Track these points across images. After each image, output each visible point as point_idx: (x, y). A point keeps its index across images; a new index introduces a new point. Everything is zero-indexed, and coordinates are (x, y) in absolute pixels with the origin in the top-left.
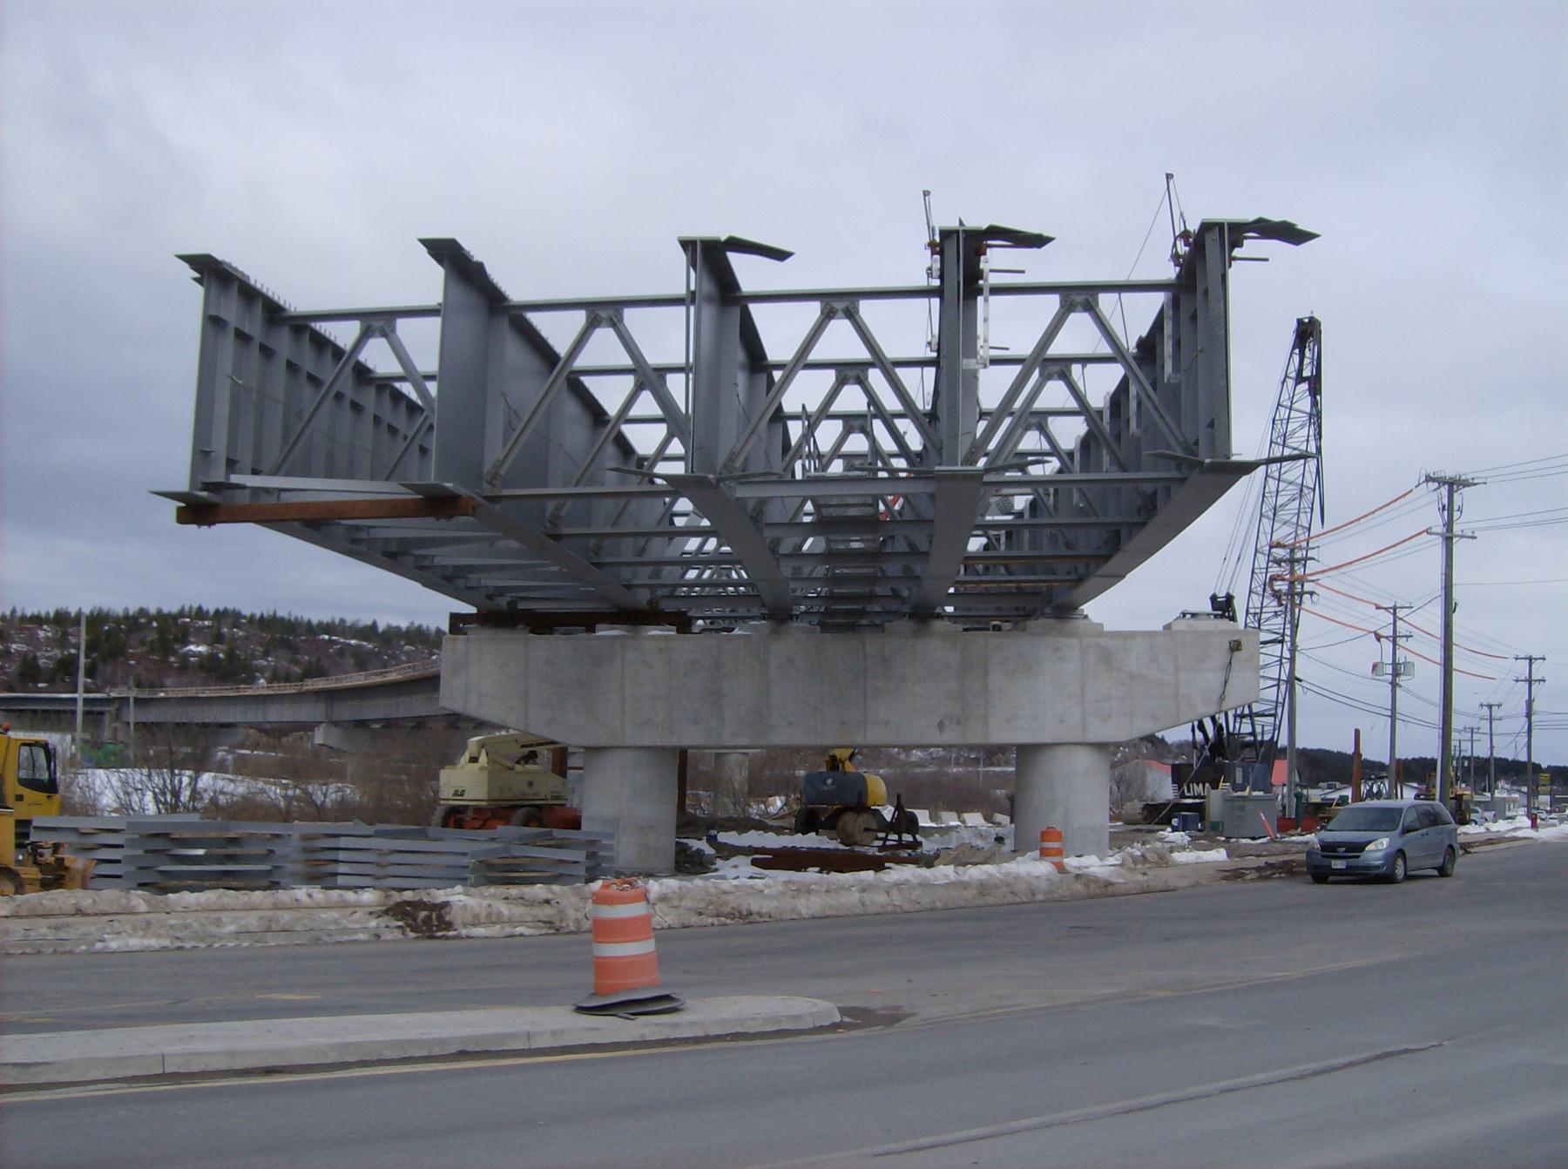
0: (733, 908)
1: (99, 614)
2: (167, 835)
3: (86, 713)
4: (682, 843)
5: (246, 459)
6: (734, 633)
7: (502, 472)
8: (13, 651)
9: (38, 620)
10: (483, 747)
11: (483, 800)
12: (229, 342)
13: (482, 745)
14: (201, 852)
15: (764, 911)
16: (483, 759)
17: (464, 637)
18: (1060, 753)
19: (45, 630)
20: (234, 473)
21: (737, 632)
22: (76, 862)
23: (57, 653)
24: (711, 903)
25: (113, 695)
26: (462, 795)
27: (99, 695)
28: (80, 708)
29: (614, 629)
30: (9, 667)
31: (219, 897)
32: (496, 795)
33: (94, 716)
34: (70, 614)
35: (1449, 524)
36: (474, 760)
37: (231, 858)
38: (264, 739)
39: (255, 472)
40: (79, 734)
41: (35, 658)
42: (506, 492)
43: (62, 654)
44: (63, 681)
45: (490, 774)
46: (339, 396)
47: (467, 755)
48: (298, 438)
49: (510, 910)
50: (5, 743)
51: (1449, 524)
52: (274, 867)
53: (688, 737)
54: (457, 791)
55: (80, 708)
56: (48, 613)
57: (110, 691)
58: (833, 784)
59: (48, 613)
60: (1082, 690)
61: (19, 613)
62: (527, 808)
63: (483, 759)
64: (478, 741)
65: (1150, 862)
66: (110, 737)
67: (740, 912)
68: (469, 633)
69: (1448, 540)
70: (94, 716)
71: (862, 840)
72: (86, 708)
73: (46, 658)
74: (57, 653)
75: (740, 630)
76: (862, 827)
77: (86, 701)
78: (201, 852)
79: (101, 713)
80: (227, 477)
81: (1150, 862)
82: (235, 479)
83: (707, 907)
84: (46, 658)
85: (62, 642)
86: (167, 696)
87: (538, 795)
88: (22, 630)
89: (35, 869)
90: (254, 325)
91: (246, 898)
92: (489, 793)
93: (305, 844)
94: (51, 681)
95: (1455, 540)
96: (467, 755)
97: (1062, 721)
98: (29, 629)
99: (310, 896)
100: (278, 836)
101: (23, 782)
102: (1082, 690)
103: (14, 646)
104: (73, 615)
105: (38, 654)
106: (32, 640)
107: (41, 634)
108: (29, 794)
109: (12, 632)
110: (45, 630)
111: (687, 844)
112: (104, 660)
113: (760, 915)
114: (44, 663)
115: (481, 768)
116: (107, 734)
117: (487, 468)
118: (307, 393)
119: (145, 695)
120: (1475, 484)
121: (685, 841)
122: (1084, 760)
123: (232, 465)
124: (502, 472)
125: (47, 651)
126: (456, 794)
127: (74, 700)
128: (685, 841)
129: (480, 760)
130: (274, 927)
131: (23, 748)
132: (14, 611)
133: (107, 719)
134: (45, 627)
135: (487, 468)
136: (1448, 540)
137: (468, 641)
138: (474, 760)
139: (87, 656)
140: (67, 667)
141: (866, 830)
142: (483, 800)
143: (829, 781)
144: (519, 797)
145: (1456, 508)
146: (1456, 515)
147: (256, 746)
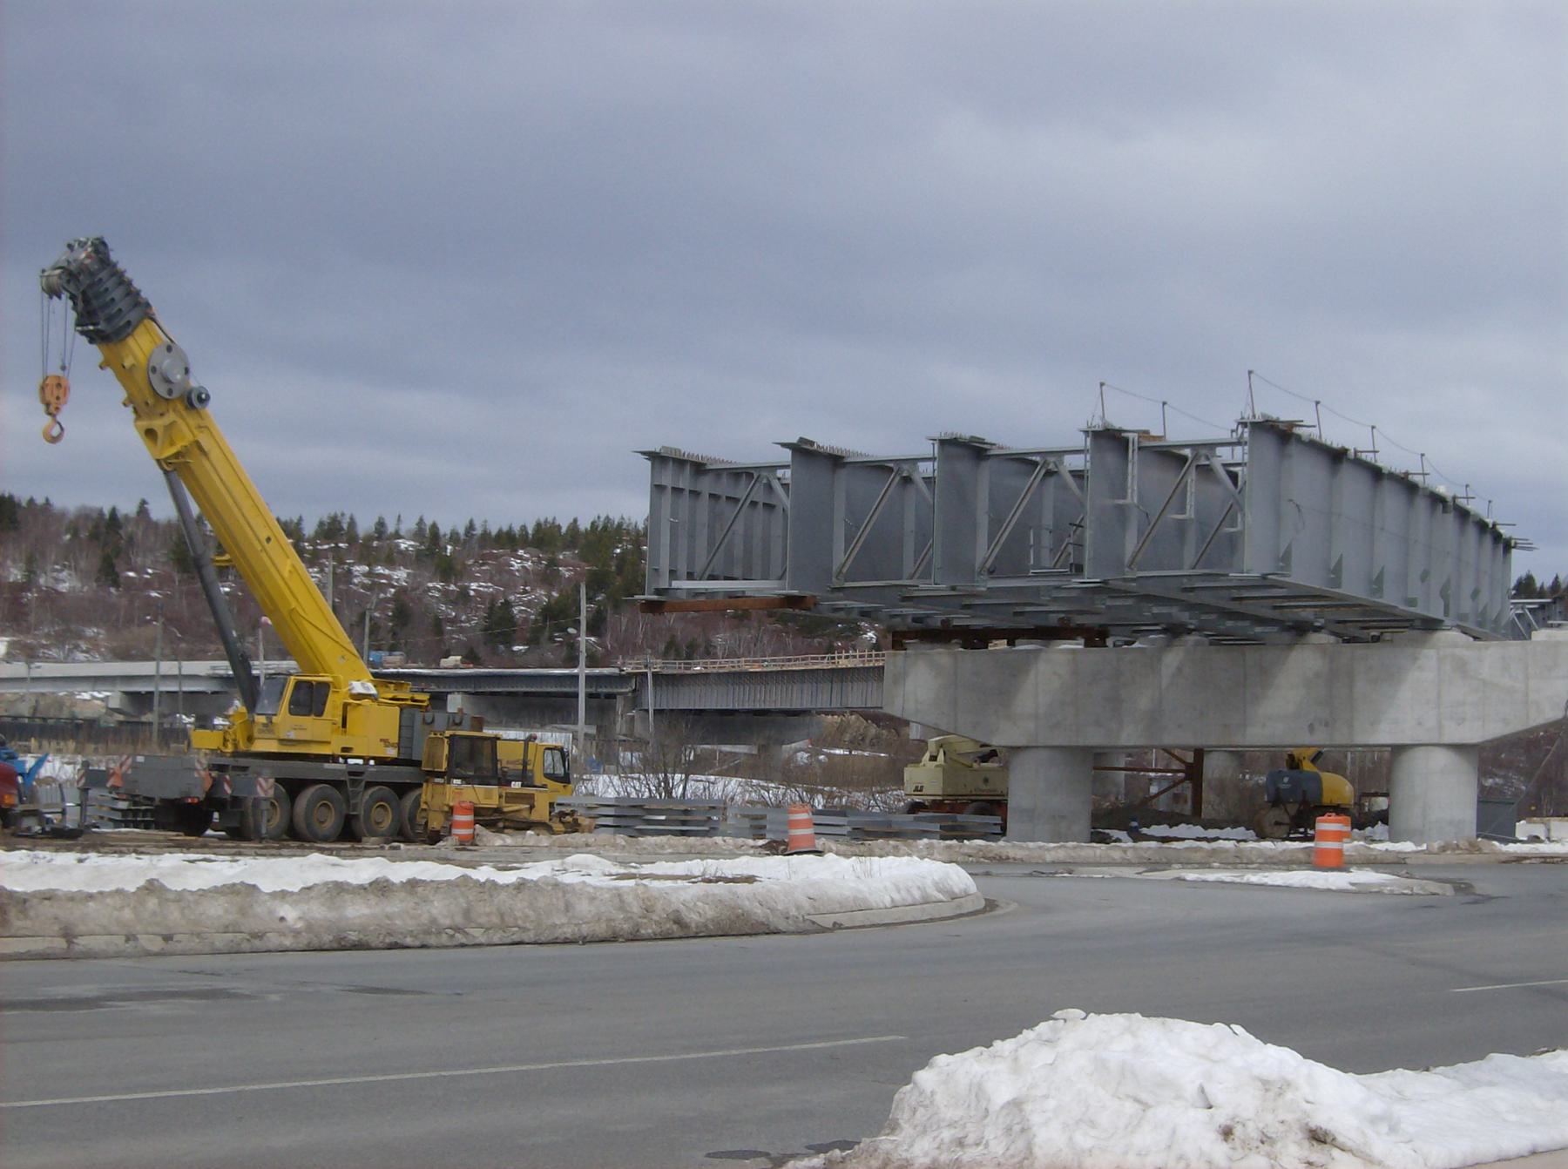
0: (996, 855)
1: (605, 528)
2: (641, 806)
3: (589, 696)
4: (1104, 833)
5: (683, 569)
6: (1134, 646)
7: (844, 570)
8: (472, 593)
9: (509, 540)
10: (941, 746)
11: (939, 795)
12: (668, 497)
13: (940, 745)
14: (663, 818)
15: (1018, 857)
16: (941, 757)
17: (904, 652)
18: (1419, 753)
19: (520, 558)
20: (675, 580)
21: (1136, 645)
22: (585, 821)
23: (541, 595)
24: (981, 851)
25: (628, 669)
26: (921, 791)
27: (606, 671)
28: (582, 691)
29: (1032, 644)
30: (468, 620)
31: (668, 840)
32: (950, 791)
33: (601, 705)
34: (559, 527)
36: (933, 758)
37: (684, 823)
38: (873, 730)
39: (690, 576)
40: (582, 727)
41: (508, 605)
42: (847, 585)
43: (549, 596)
44: (551, 639)
45: (945, 771)
46: (754, 504)
47: (927, 756)
48: (721, 543)
49: (837, 847)
50: (535, 747)
52: (711, 828)
53: (1094, 738)
54: (917, 787)
55: (582, 691)
56: (524, 528)
57: (624, 664)
58: (1288, 783)
59: (524, 528)
60: (1439, 696)
61: (478, 531)
62: (980, 803)
63: (941, 757)
64: (936, 741)
65: (1461, 849)
66: (624, 731)
67: (1000, 857)
68: (908, 647)
70: (601, 705)
71: (1272, 833)
72: (590, 690)
73: (526, 603)
74: (541, 593)
75: (1140, 643)
76: (1274, 821)
77: (588, 677)
78: (663, 818)
79: (611, 696)
80: (670, 585)
81: (1461, 849)
82: (675, 584)
83: (978, 853)
84: (526, 603)
85: (547, 577)
86: (704, 671)
87: (995, 791)
88: (485, 558)
89: (561, 825)
90: (685, 482)
91: (685, 841)
92: (944, 789)
93: (762, 822)
94: (533, 641)
96: (927, 756)
97: (1420, 724)
98: (496, 557)
99: (725, 841)
100: (714, 808)
101: (548, 776)
102: (1439, 696)
103: (474, 586)
104: (564, 530)
105: (512, 598)
106: (501, 574)
107: (516, 564)
108: (551, 783)
109: (470, 562)
110: (520, 558)
111: (1108, 834)
112: (617, 607)
113: (1015, 859)
114: (521, 611)
115: (937, 766)
116: (620, 726)
117: (835, 568)
118: (729, 511)
119: (675, 667)
121: (1107, 831)
122: (1441, 759)
123: (673, 574)
124: (844, 570)
125: (525, 592)
126: (916, 790)
127: (576, 677)
128: (1107, 831)
129: (938, 759)
130: (693, 851)
131: (547, 751)
132: (471, 527)
133: (620, 705)
134: (521, 552)
135: (835, 568)
137: (906, 656)
138: (933, 758)
139: (590, 600)
140: (557, 616)
141: (1277, 823)
142: (939, 795)
143: (1286, 780)
144: (974, 793)
147: (854, 744)
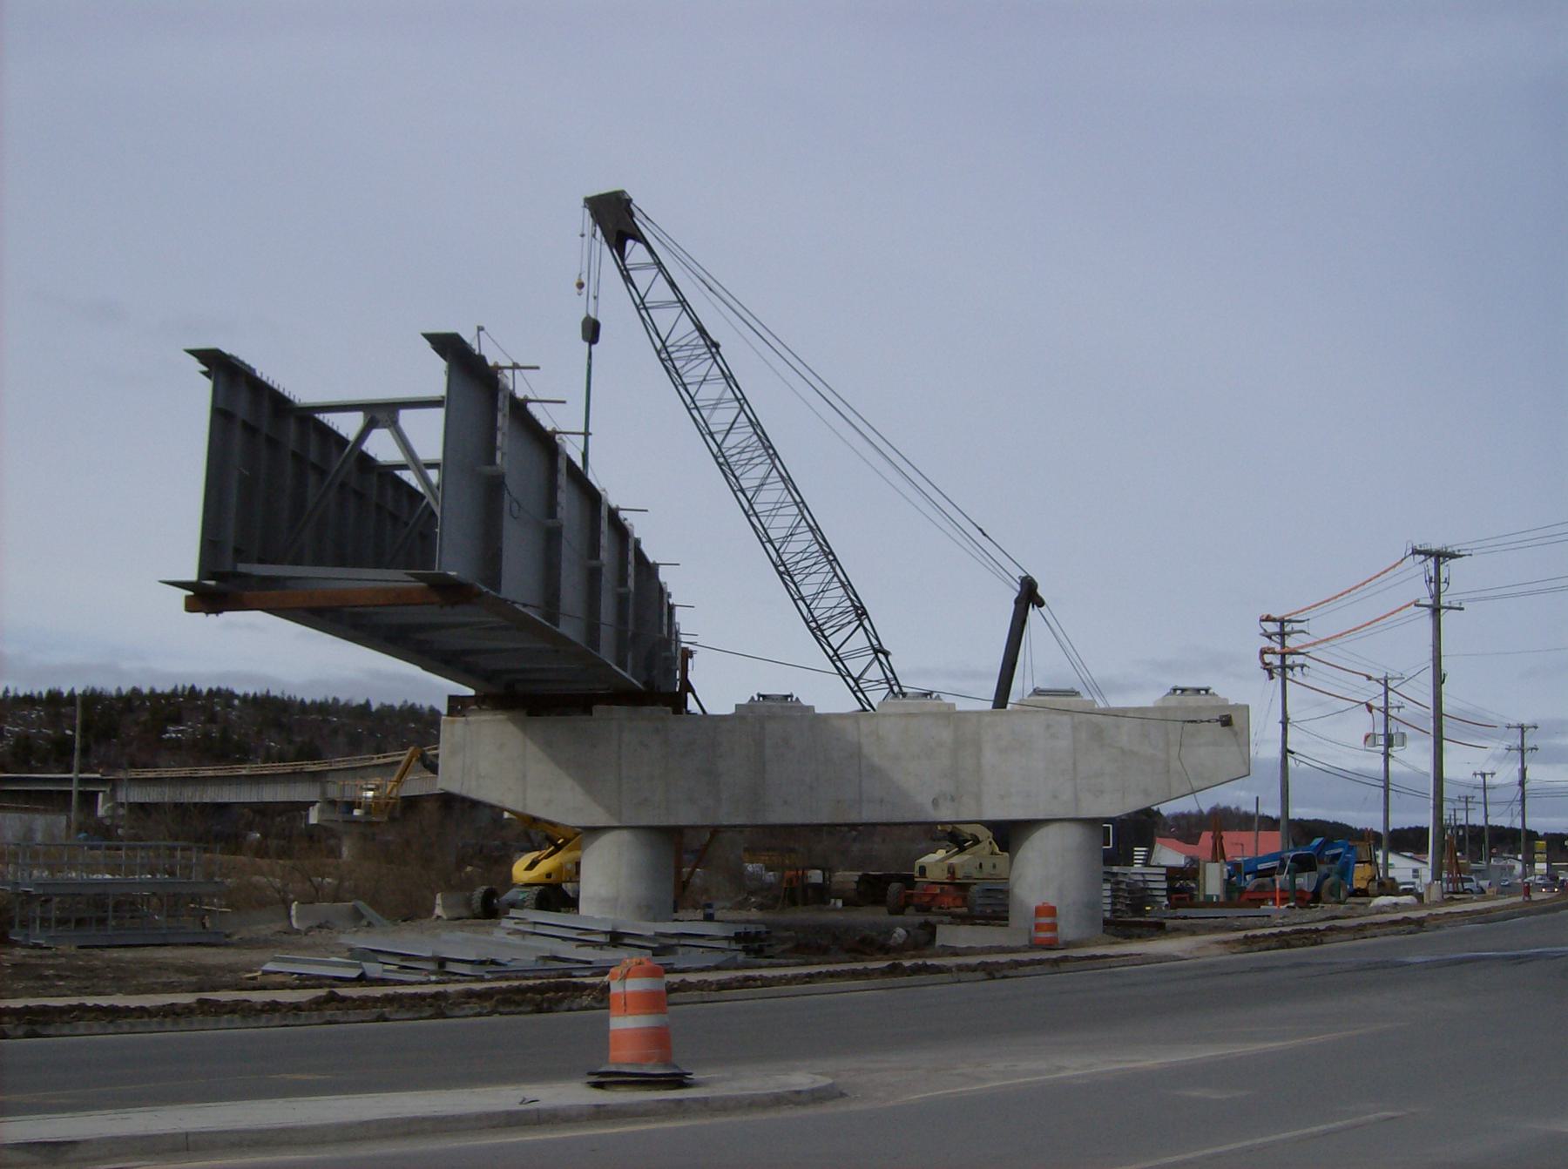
35: (1437, 596)
51: (1437, 596)
69: (1436, 610)
95: (1442, 611)
120: (1461, 556)
136: (1436, 610)
145: (1442, 580)
146: (1443, 586)
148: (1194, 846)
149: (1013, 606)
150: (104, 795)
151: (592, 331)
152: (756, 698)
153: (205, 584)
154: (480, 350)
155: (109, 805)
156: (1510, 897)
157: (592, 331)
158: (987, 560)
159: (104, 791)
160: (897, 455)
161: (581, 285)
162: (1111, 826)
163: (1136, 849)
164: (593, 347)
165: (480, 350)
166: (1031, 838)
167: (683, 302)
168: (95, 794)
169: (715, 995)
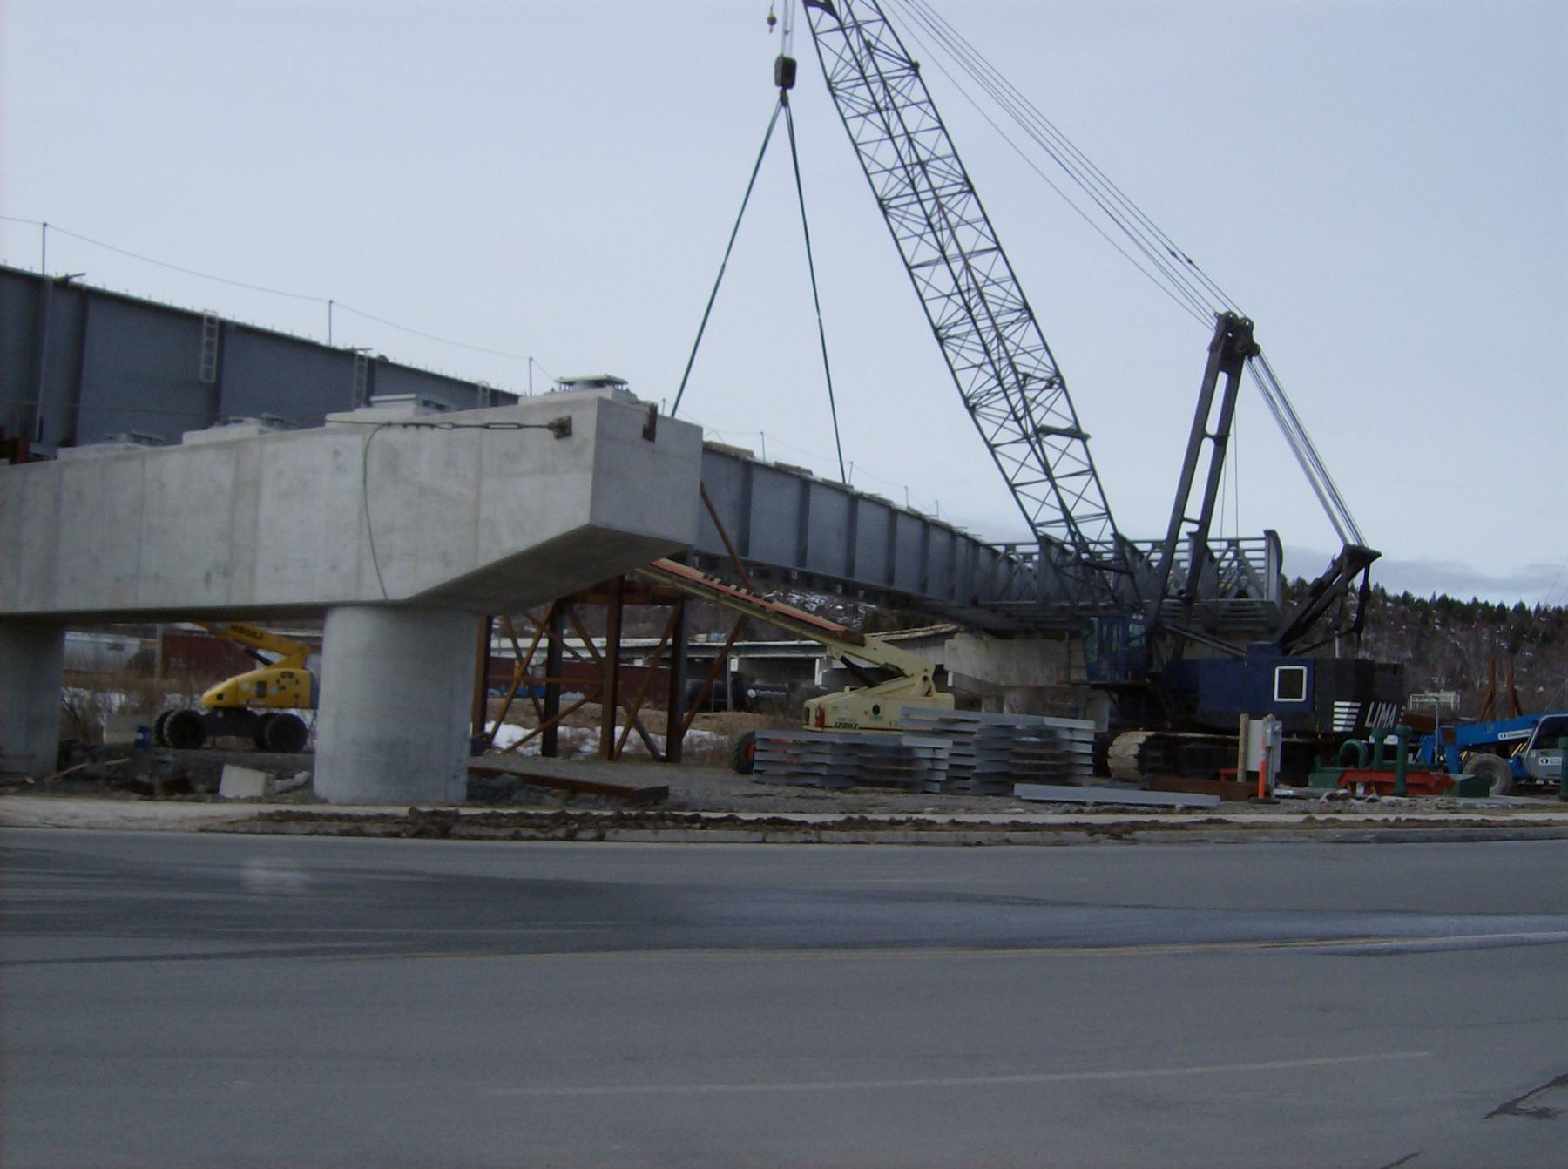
148: (320, 428)
149: (1207, 354)
150: (820, 662)
151: (786, 73)
152: (557, 389)
153: (1269, 641)
154: (1331, 500)
155: (825, 671)
156: (816, 718)
157: (786, 73)
158: (1201, 313)
159: (822, 658)
160: (1097, 167)
161: (772, 21)
162: (1305, 669)
163: (1337, 703)
164: (789, 92)
165: (1331, 500)
166: (526, 548)
167: (885, 20)
168: (814, 660)
169: (813, 836)
